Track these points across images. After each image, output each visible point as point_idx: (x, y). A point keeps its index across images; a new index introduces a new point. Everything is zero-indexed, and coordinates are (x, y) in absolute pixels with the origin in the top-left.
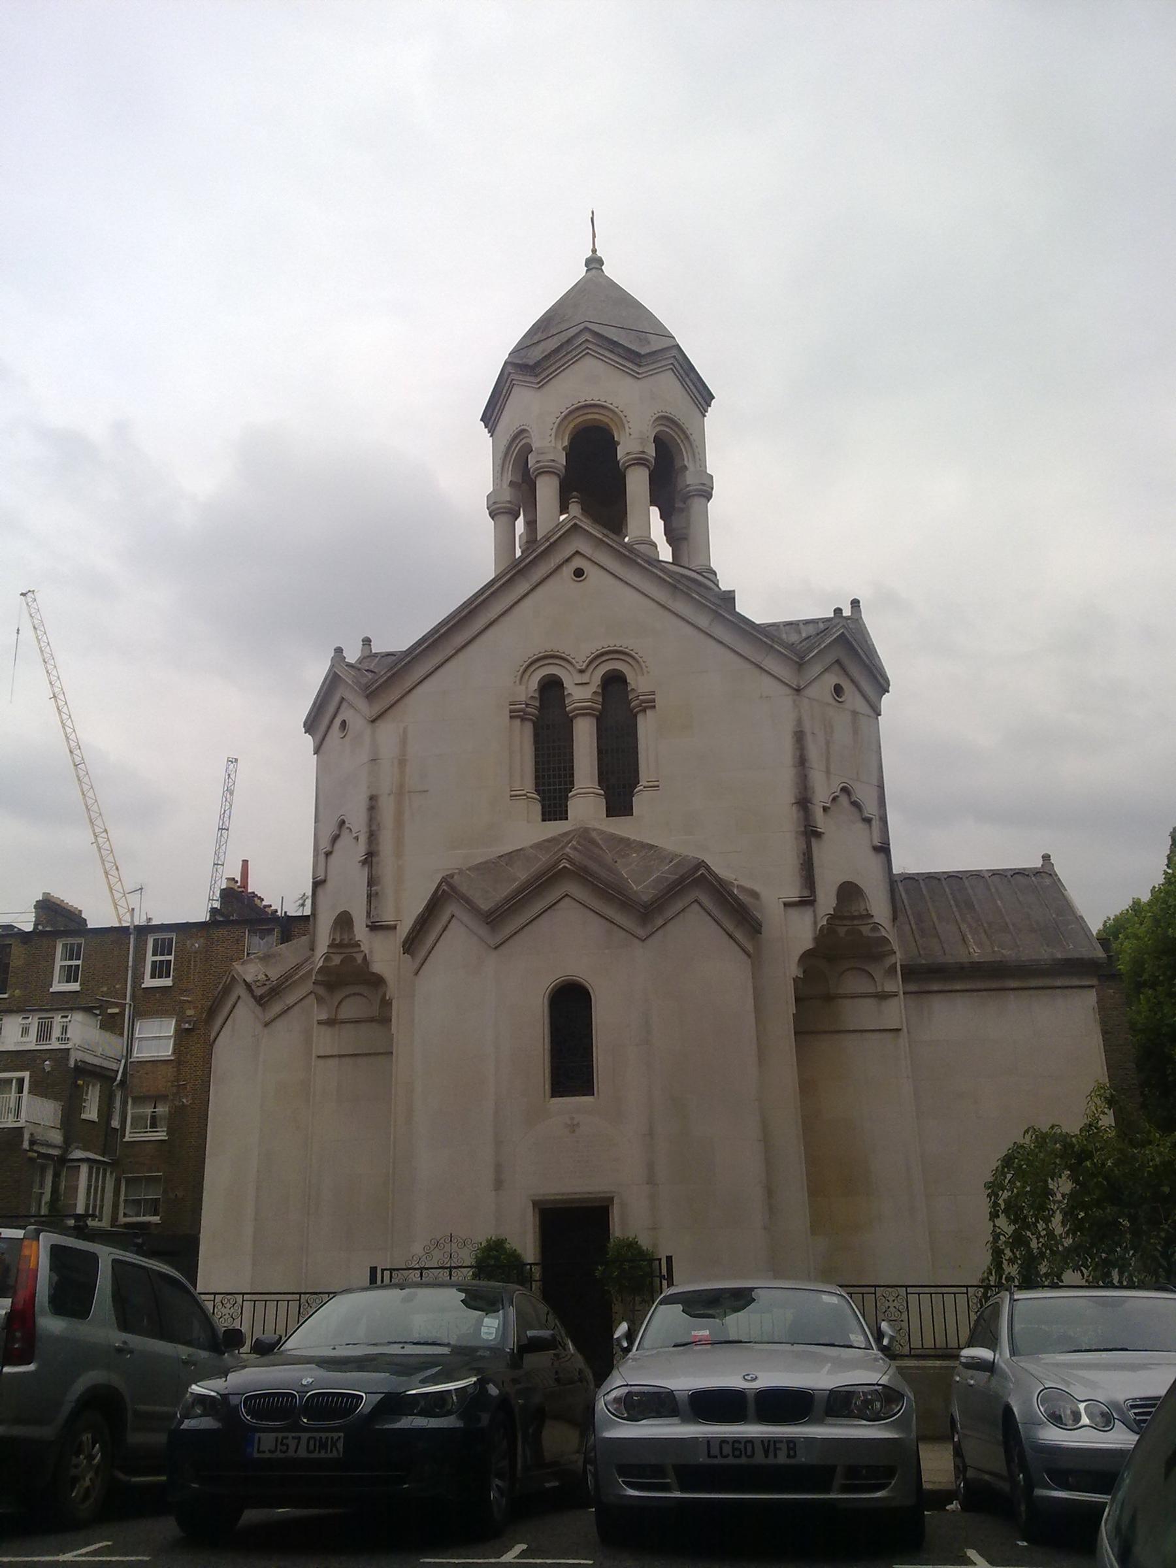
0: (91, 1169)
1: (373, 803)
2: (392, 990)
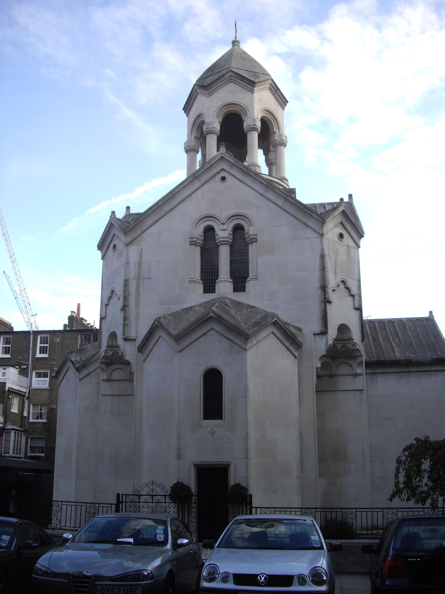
0: (15, 433)
2: (134, 367)
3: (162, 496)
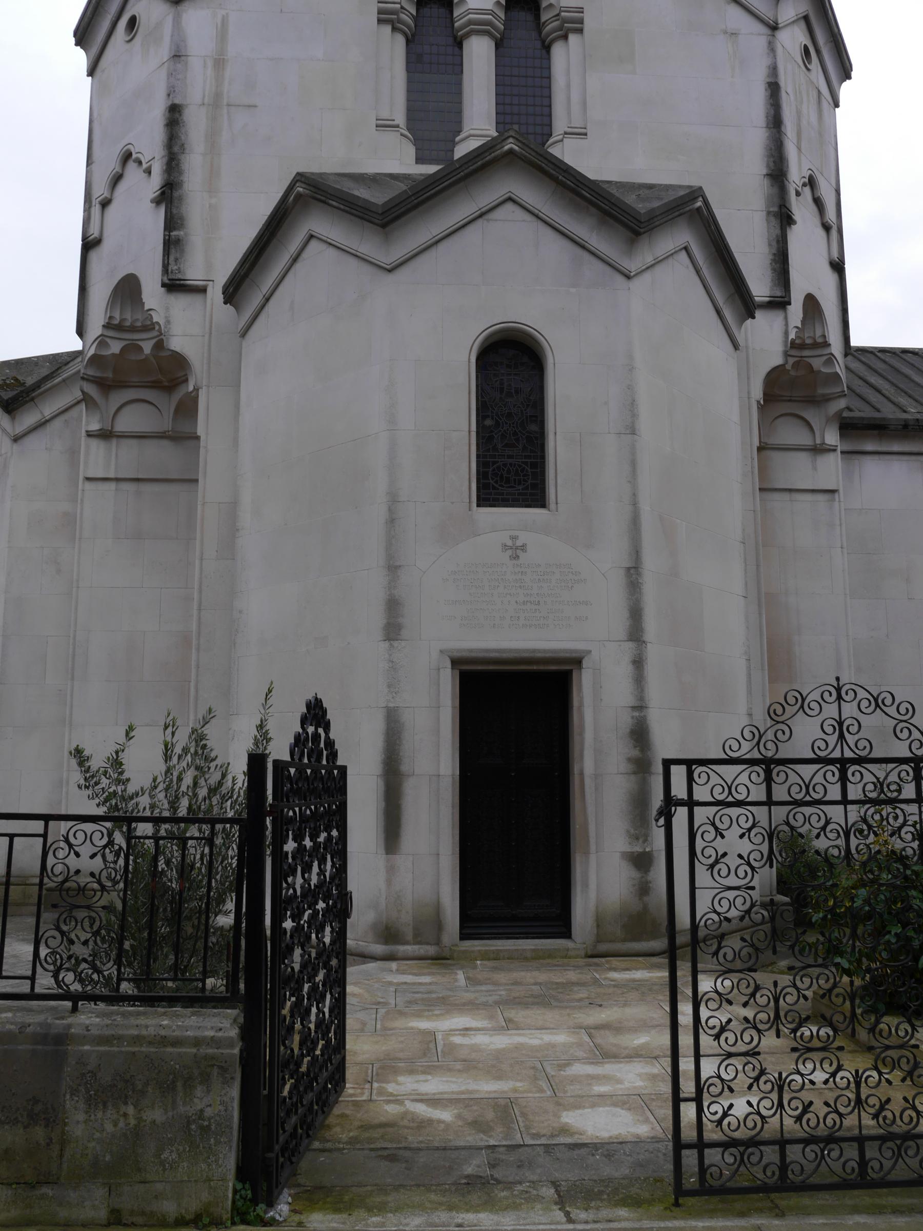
1: (174, 116)
3: (752, 762)
